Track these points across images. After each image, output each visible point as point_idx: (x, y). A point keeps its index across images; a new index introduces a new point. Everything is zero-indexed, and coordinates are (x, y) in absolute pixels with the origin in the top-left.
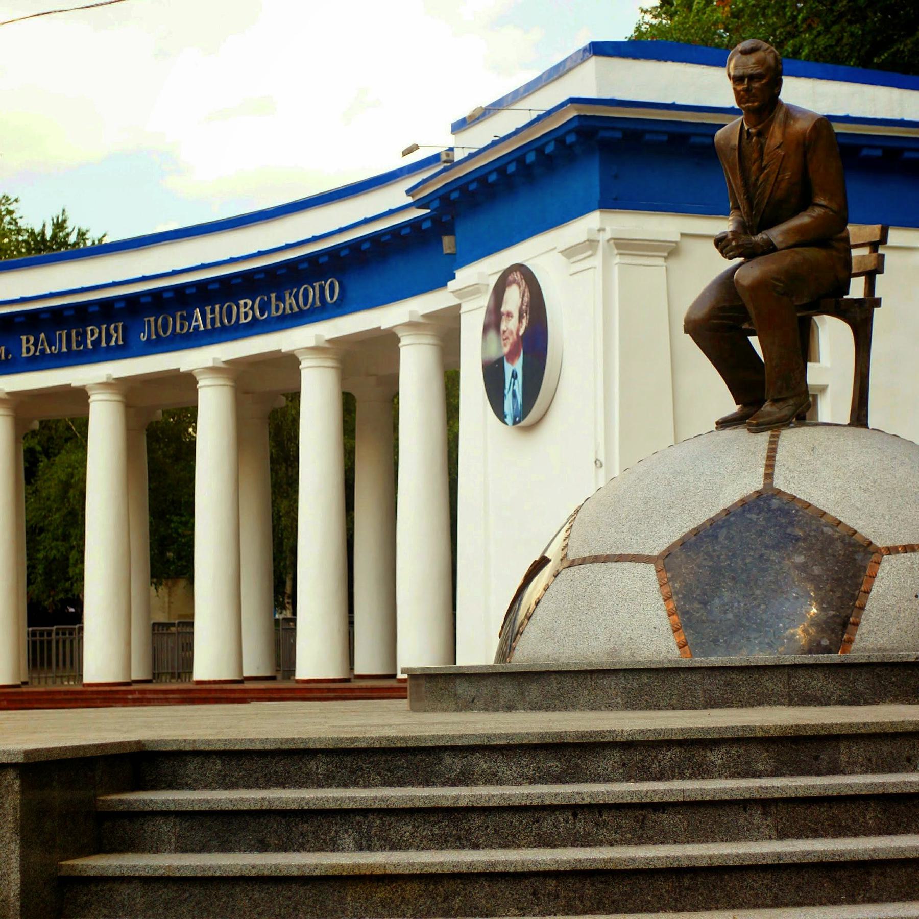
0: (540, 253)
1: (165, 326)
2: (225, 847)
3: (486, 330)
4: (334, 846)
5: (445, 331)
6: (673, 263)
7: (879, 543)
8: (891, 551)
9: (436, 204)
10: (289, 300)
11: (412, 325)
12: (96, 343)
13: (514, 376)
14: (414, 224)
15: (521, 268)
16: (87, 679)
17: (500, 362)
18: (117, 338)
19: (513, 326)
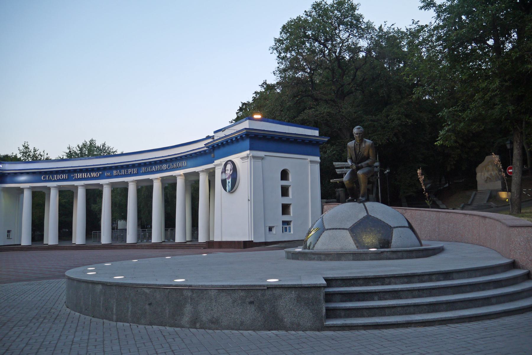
0: (235, 158)
1: (146, 169)
2: (351, 301)
3: (222, 173)
4: (373, 300)
5: (211, 174)
6: (263, 161)
7: (392, 226)
8: (395, 227)
9: (211, 147)
10: (175, 165)
11: (202, 171)
12: (131, 173)
13: (229, 182)
14: (205, 151)
15: (230, 161)
16: (127, 242)
17: (226, 179)
18: (135, 172)
19: (229, 172)
